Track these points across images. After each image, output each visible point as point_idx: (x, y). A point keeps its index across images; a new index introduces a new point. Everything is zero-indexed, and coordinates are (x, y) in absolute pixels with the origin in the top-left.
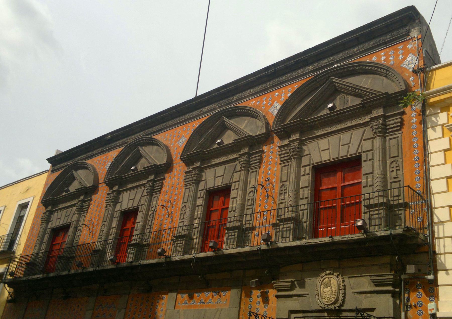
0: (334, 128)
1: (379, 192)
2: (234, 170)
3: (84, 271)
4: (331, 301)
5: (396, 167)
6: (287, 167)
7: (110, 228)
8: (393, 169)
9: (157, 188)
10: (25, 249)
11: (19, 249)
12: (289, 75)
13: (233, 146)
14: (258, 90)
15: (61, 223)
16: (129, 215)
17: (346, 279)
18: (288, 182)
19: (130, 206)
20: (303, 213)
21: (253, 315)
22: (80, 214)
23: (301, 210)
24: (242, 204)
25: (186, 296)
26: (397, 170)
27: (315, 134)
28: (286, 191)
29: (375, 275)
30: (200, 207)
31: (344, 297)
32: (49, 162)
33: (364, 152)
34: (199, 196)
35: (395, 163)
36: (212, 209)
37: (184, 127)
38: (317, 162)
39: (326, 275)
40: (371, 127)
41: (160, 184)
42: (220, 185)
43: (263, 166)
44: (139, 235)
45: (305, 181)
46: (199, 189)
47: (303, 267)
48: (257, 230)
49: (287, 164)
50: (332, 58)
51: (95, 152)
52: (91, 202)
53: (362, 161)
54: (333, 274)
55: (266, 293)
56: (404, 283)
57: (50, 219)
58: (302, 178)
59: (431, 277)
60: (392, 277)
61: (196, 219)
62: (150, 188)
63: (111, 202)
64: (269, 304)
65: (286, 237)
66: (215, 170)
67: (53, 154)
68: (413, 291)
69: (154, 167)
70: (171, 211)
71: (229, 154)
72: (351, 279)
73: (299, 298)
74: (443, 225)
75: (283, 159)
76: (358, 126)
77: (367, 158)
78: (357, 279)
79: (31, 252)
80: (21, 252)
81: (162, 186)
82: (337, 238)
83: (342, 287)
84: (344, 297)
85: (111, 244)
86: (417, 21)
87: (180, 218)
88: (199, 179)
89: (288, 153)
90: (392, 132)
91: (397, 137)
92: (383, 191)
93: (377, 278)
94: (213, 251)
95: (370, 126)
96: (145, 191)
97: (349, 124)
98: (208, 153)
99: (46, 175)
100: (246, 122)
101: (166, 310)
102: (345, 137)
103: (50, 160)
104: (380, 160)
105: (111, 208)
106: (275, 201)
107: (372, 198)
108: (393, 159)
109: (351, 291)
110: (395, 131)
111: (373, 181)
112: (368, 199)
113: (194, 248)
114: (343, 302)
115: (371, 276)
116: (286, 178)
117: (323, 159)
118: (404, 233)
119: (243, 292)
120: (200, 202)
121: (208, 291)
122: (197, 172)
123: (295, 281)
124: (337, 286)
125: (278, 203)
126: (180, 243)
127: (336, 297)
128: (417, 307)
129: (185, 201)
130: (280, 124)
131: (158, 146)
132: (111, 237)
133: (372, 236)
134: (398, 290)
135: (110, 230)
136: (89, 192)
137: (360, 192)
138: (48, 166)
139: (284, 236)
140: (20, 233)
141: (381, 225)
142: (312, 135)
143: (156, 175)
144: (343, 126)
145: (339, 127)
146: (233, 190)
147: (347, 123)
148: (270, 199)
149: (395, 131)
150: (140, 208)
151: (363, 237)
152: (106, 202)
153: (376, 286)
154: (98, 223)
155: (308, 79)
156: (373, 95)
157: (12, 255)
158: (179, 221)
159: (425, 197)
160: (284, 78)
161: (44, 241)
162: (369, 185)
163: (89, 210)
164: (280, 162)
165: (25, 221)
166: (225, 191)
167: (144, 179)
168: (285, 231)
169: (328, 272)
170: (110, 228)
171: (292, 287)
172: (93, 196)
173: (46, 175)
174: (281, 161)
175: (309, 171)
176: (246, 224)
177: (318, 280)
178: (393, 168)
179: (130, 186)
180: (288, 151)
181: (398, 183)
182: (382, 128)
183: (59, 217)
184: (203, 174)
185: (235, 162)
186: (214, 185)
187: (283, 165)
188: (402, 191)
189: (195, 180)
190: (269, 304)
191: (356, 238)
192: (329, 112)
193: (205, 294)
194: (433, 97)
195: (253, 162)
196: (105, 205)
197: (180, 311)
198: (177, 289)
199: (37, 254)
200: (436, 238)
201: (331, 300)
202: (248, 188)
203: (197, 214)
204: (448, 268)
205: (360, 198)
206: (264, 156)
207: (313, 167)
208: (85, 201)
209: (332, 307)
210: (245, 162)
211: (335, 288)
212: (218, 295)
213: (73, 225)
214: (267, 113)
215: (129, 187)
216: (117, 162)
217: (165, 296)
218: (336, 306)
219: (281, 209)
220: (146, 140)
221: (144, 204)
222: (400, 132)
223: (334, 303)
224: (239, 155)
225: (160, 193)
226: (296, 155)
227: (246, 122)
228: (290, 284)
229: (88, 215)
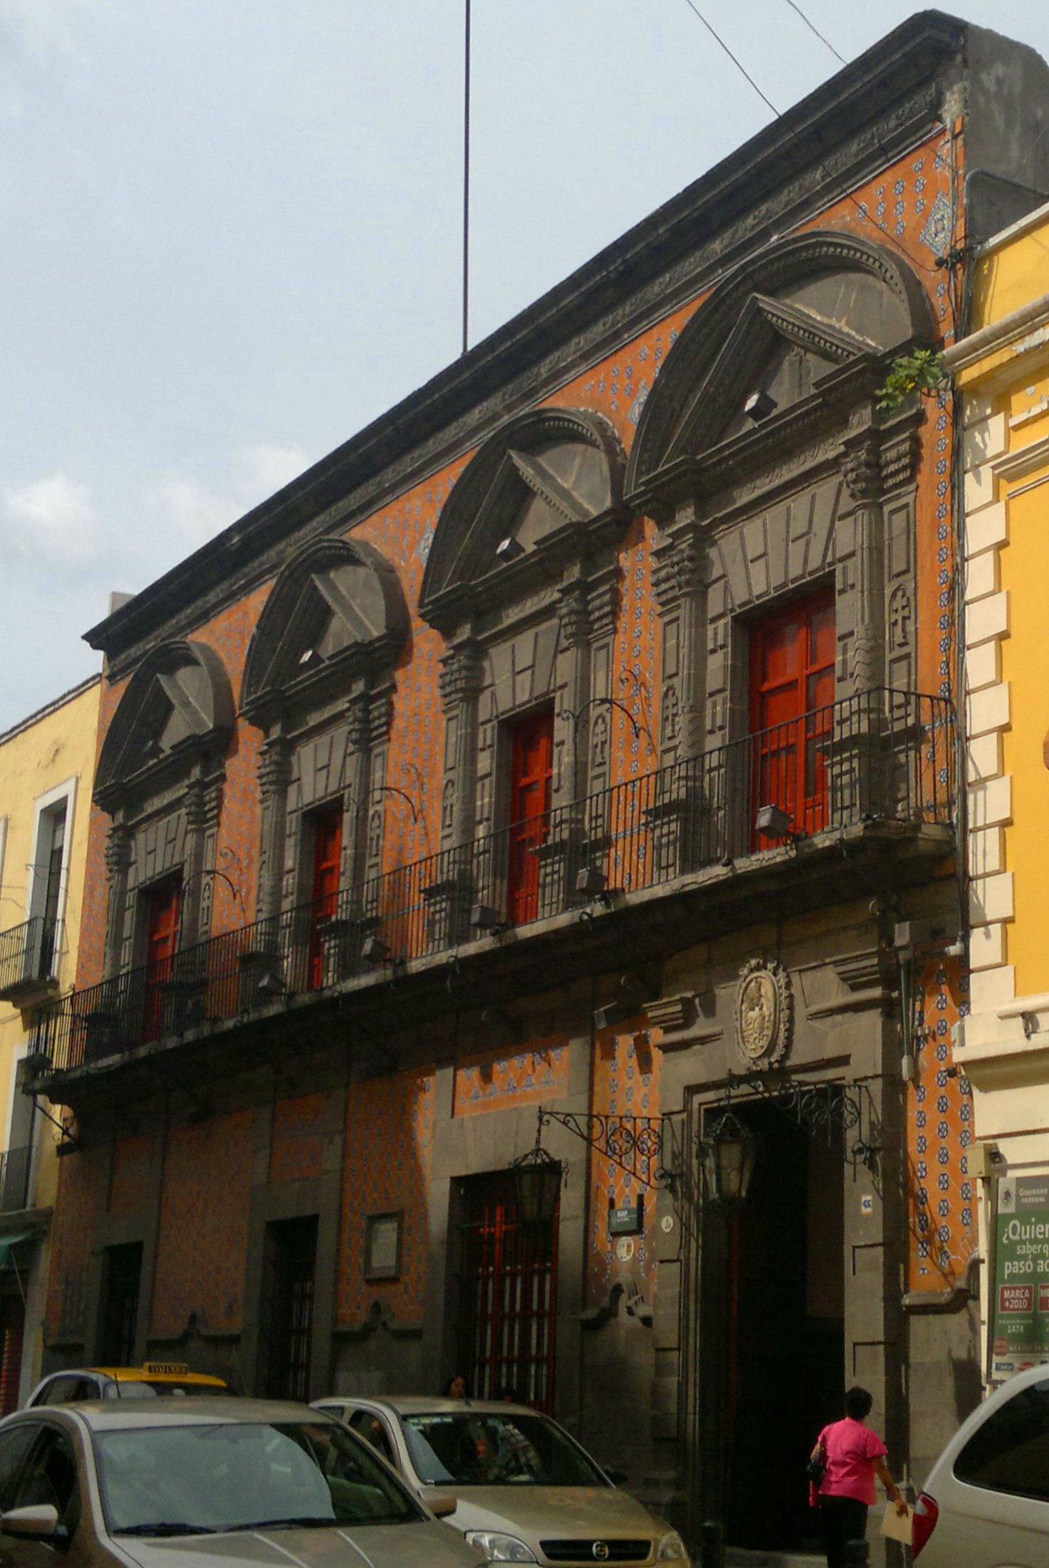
3: (217, 1031)
9: (892, 468)
10: (81, 967)
11: (68, 971)
12: (667, 276)
14: (599, 339)
15: (159, 869)
16: (527, 731)
18: (911, 575)
19: (523, 697)
21: (553, 1120)
22: (200, 832)
25: (474, 1072)
28: (906, 613)
29: (842, 960)
30: (487, 781)
31: (790, 1031)
32: (95, 647)
34: (480, 745)
37: (625, 357)
39: (752, 971)
41: (383, 710)
42: (322, 798)
43: (623, 623)
46: (481, 719)
48: (620, 844)
50: (763, 208)
51: (212, 598)
52: (923, 431)
56: (908, 973)
57: (129, 855)
59: (954, 950)
60: (875, 961)
61: (480, 822)
62: (357, 726)
63: (456, 691)
65: (668, 866)
67: (100, 613)
68: (930, 995)
69: (192, 745)
70: (422, 802)
74: (985, 789)
79: (99, 975)
80: (74, 981)
81: (390, 715)
82: (745, 864)
83: (784, 1004)
84: (790, 1031)
85: (289, 926)
86: (959, 58)
87: (444, 822)
88: (473, 684)
90: (896, 486)
93: (864, 964)
94: (493, 935)
96: (846, 492)
99: (95, 693)
100: (577, 461)
101: (435, 1123)
103: (95, 638)
104: (862, 592)
105: (685, 611)
114: (788, 1046)
115: (835, 963)
118: (868, 834)
120: (485, 763)
121: (520, 1052)
122: (464, 662)
123: (694, 997)
124: (772, 1000)
126: (554, 872)
128: (938, 1037)
131: (856, 267)
132: (286, 905)
134: (895, 994)
135: (281, 879)
136: (212, 748)
138: (95, 661)
139: (664, 864)
140: (59, 916)
141: (854, 805)
143: (590, 562)
148: (643, 741)
150: (838, 574)
152: (258, 781)
153: (855, 988)
154: (251, 861)
155: (698, 303)
157: (50, 992)
158: (441, 834)
159: (951, 703)
160: (656, 289)
161: (710, 687)
163: (224, 815)
164: (659, 609)
165: (68, 870)
166: (810, 600)
169: (753, 962)
170: (279, 875)
171: (688, 1019)
172: (228, 763)
173: (95, 693)
175: (726, 636)
179: (745, 496)
182: (867, 479)
183: (150, 849)
184: (713, 553)
186: (751, 594)
187: (667, 619)
189: (462, 690)
193: (516, 1062)
194: (967, 366)
196: (259, 796)
198: (451, 1055)
199: (113, 982)
203: (482, 806)
204: (989, 918)
206: (625, 587)
208: (373, 699)
209: (764, 1065)
210: (574, 618)
213: (564, 702)
214: (920, 245)
215: (312, 724)
217: (430, 1081)
218: (773, 1060)
219: (711, 753)
220: (330, 547)
221: (852, 555)
222: (912, 487)
223: (768, 1052)
224: (845, 443)
225: (389, 740)
227: (577, 461)
228: (679, 1008)
229: (223, 831)
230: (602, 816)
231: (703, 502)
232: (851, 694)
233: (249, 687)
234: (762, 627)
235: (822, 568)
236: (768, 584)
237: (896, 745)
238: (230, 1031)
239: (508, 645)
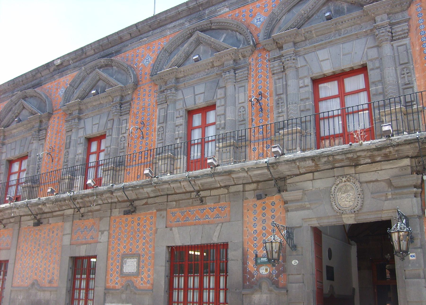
5: (407, 73)
8: (404, 76)
100: (224, 36)
108: (403, 66)
116: (281, 90)
129: (161, 121)
181: (162, 144)
200: (91, 279)
202: (237, 103)
227: (224, 36)
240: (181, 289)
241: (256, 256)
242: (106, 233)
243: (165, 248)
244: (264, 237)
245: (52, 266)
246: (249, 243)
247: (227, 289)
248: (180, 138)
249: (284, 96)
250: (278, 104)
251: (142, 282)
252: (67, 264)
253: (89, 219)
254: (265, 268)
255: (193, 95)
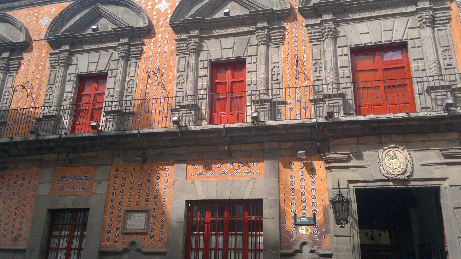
0: (373, 14)
1: (332, 84)
2: (248, 43)
4: (400, 172)
6: (319, 46)
7: (62, 92)
13: (245, 18)
17: (412, 153)
20: (202, 103)
23: (200, 99)
24: (266, 78)
25: (200, 167)
26: (277, 74)
27: (349, 17)
28: (133, 86)
33: (249, 56)
35: (276, 68)
36: (217, 81)
38: (365, 42)
39: (389, 148)
40: (419, 17)
41: (18, 63)
44: (68, 106)
45: (70, 87)
47: (358, 141)
49: (319, 43)
52: (22, 62)
53: (247, 63)
54: (398, 148)
55: (311, 164)
58: (339, 59)
61: (201, 90)
64: (316, 174)
66: (89, 56)
71: (238, 26)
72: (416, 153)
73: (357, 169)
75: (53, 65)
76: (401, 15)
77: (251, 61)
78: (423, 152)
83: (409, 159)
89: (57, 60)
90: (440, 24)
91: (446, 29)
92: (337, 84)
95: (418, 16)
97: (389, 12)
98: (210, 23)
101: (174, 182)
102: (388, 23)
106: (307, 77)
107: (110, 106)
108: (49, 86)
109: (420, 163)
110: (443, 23)
111: (114, 93)
112: (253, 95)
113: (204, 119)
114: (412, 172)
117: (90, 70)
119: (280, 163)
120: (203, 72)
121: (233, 162)
125: (312, 80)
127: (405, 168)
130: (52, 34)
131: (128, 7)
133: (454, 113)
135: (63, 94)
137: (103, 100)
142: (345, 17)
144: (383, 12)
145: (377, 13)
146: (109, 77)
147: (386, 10)
149: (443, 23)
151: (94, 135)
153: (446, 158)
156: (124, 26)
162: (345, 77)
164: (49, 67)
166: (100, 77)
167: (113, 41)
168: (184, 116)
169: (392, 145)
171: (349, 159)
174: (310, 40)
175: (74, 79)
176: (126, 109)
177: (380, 153)
178: (445, 56)
179: (86, 47)
180: (57, 58)
181: (182, 93)
185: (247, 35)
188: (133, 104)
189: (194, 49)
190: (316, 174)
191: (437, 115)
192: (92, 32)
195: (134, 53)
197: (195, 182)
201: (399, 170)
205: (102, 105)
207: (77, 75)
209: (402, 177)
210: (265, 36)
211: (402, 160)
212: (247, 166)
215: (86, 48)
216: (63, 18)
219: (106, 102)
222: (449, 25)
223: (403, 174)
226: (331, 35)
228: (347, 156)
230: (4, 116)
231: (73, 45)
232: (162, 96)
233: (50, 31)
234: (83, 80)
235: (105, 70)
236: (232, 55)
237: (277, 104)
238: (135, 134)
239: (234, 38)
240: (219, 249)
241: (295, 215)
242: (105, 184)
243: (184, 203)
244: (303, 196)
245: (19, 219)
246: (286, 201)
247: (82, 249)
248: (204, 89)
249: (185, 74)
250: (316, 68)
251: (152, 240)
252: (43, 217)
253: (79, 166)
254: (305, 228)
255: (219, 48)
